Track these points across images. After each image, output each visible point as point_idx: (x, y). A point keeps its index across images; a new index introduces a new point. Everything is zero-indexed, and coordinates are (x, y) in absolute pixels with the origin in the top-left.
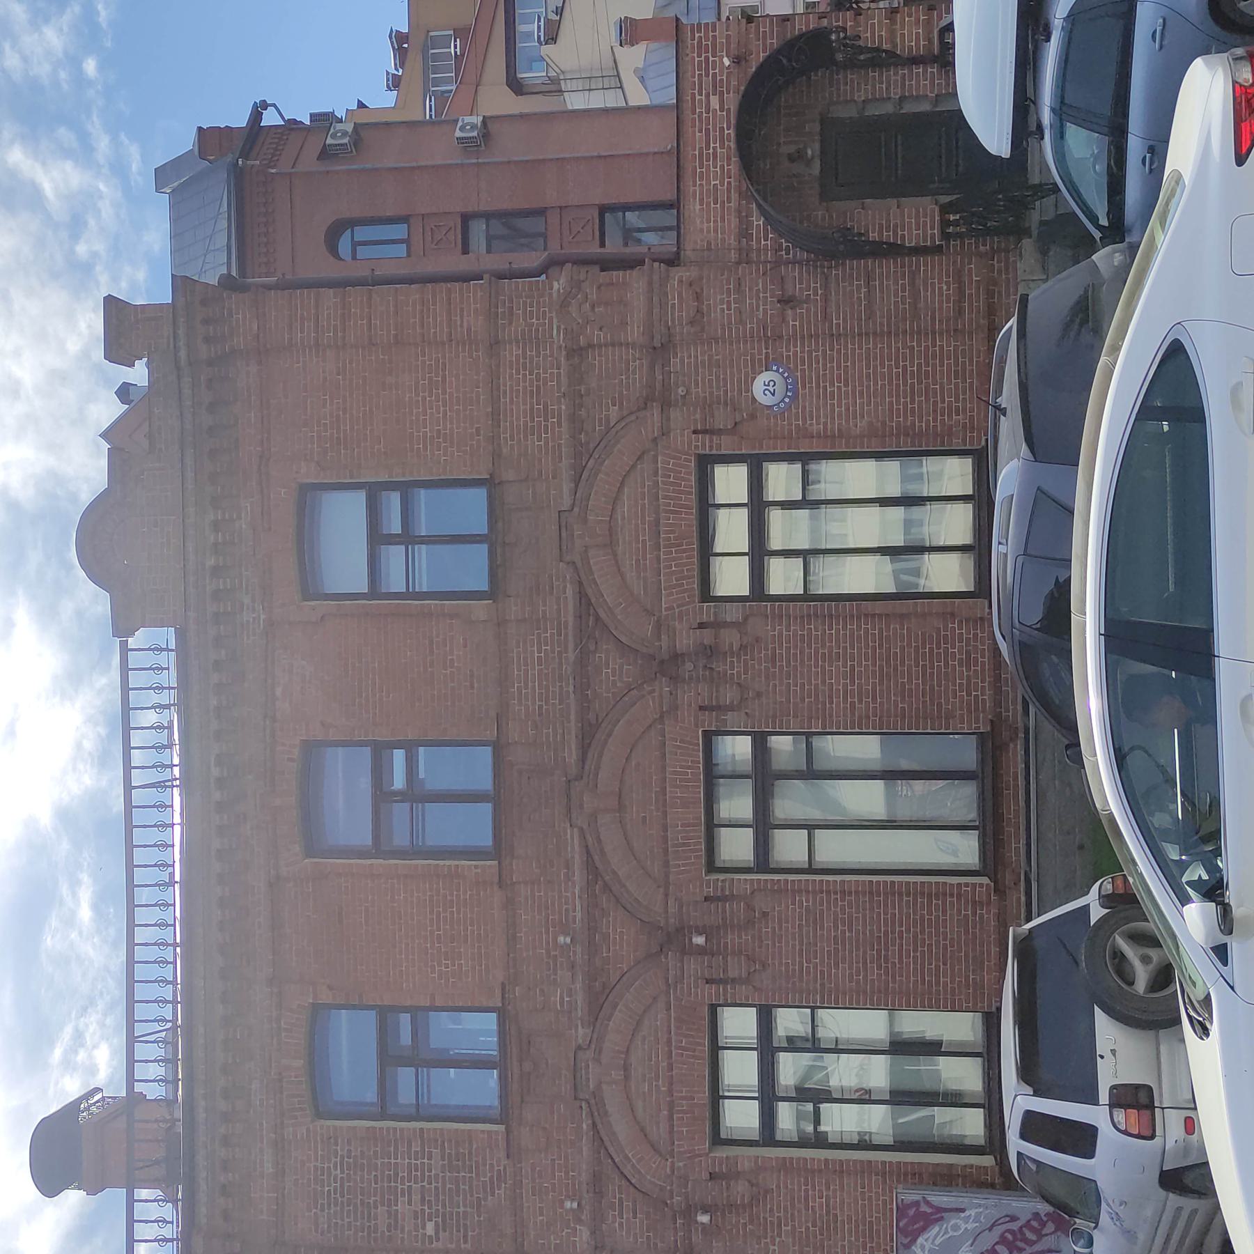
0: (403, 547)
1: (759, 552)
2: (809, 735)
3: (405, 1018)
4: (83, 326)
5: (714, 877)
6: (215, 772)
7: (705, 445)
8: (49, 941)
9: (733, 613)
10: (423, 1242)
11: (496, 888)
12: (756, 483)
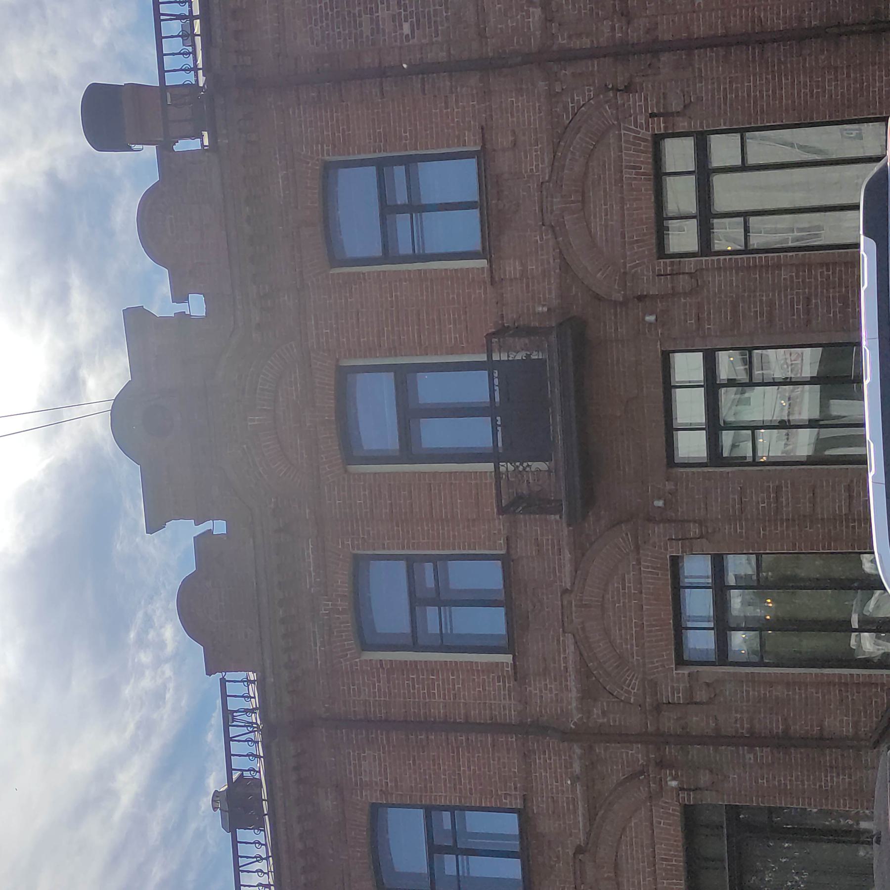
0: (409, 215)
1: (706, 215)
2: (751, 350)
3: (429, 567)
4: (105, 21)
5: (685, 671)
6: (299, 846)
7: (660, 126)
8: (118, 547)
9: (690, 264)
10: (402, 41)
11: (488, 285)
12: (702, 152)
